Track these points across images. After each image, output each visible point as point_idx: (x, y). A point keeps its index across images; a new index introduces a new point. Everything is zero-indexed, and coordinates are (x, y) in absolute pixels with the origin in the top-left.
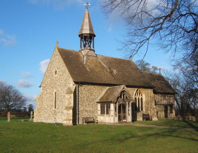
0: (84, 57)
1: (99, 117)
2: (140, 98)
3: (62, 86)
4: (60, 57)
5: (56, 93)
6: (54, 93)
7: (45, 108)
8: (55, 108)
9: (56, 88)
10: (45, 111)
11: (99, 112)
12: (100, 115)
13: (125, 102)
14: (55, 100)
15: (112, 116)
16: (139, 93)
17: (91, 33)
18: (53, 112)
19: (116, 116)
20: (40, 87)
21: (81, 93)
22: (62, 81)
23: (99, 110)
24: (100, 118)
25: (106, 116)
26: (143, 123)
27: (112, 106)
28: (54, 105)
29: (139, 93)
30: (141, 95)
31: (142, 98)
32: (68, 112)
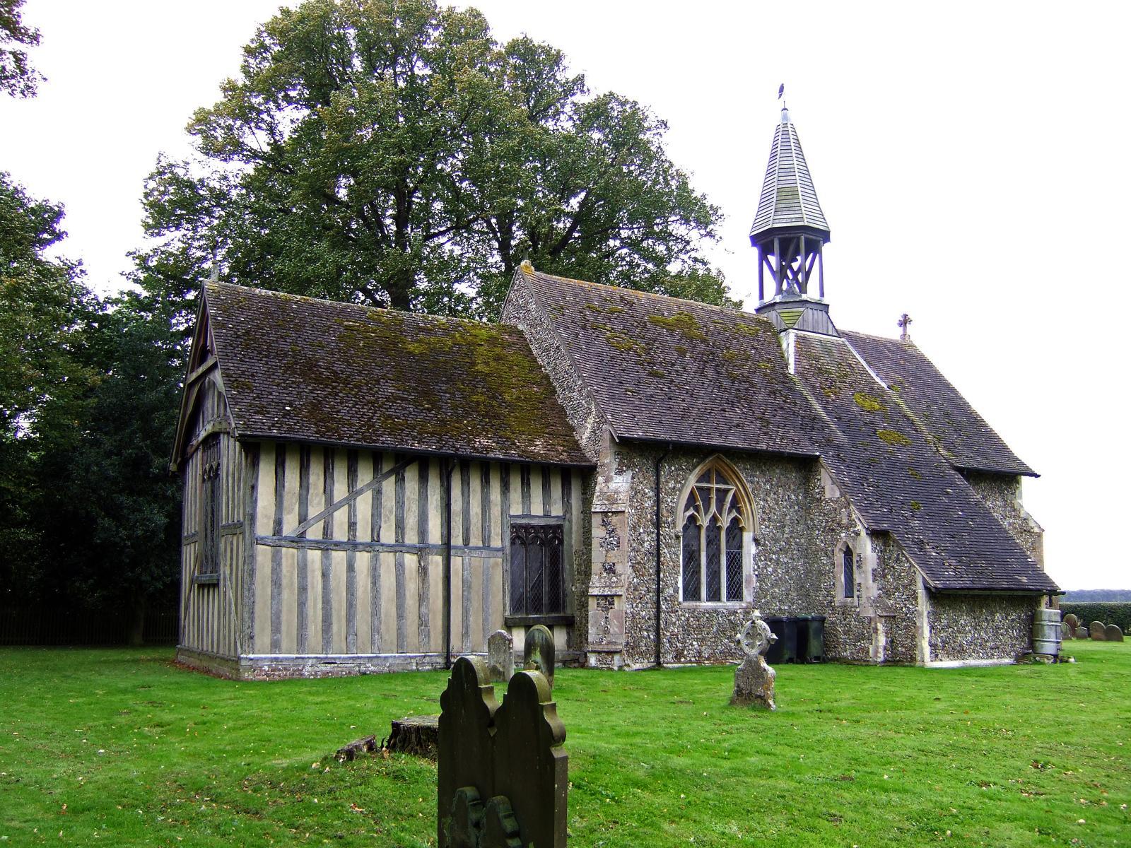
2: (725, 522)
16: (714, 496)
17: (184, 542)
29: (714, 496)
30: (735, 504)
31: (735, 521)
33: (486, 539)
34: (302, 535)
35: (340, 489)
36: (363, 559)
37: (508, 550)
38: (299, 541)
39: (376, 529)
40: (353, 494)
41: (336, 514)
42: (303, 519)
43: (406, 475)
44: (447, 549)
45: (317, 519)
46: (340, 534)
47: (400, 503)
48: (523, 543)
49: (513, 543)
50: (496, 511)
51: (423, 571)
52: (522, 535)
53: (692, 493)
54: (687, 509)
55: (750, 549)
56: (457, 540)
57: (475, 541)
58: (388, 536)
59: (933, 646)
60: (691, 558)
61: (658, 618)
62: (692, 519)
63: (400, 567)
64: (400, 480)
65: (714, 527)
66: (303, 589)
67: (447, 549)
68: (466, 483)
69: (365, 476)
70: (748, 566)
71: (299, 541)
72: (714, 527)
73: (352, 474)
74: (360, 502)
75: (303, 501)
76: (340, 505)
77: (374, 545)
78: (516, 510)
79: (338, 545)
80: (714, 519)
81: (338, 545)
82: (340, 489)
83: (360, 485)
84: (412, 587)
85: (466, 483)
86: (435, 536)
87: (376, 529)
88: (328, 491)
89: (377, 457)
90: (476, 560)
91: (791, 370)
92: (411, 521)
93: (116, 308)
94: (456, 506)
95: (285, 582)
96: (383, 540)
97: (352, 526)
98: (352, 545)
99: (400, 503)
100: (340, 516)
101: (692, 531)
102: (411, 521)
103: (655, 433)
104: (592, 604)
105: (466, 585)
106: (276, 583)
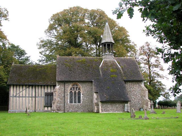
2: (77, 92)
31: (79, 91)
33: (41, 95)
34: (16, 96)
35: (21, 90)
36: (24, 98)
37: (44, 97)
38: (16, 96)
39: (26, 95)
40: (23, 90)
41: (19, 92)
42: (16, 94)
43: (49, 88)
44: (35, 97)
45: (18, 94)
46: (21, 95)
47: (29, 91)
48: (47, 96)
49: (45, 96)
50: (43, 92)
51: (32, 100)
52: (47, 94)
53: (71, 87)
54: (70, 90)
55: (82, 95)
56: (37, 96)
57: (40, 96)
58: (27, 95)
59: (102, 110)
60: (71, 97)
61: (64, 105)
62: (71, 91)
63: (29, 99)
64: (29, 88)
65: (75, 93)
66: (16, 102)
67: (35, 97)
68: (38, 88)
69: (24, 88)
70: (81, 98)
71: (16, 96)
72: (75, 93)
73: (23, 88)
74: (24, 92)
75: (16, 92)
76: (21, 92)
77: (26, 97)
78: (46, 91)
79: (21, 97)
80: (75, 91)
81: (21, 97)
82: (21, 90)
83: (24, 89)
84: (31, 102)
85: (38, 88)
86: (34, 95)
87: (26, 95)
88: (19, 90)
89: (26, 86)
90: (40, 98)
91: (100, 66)
92: (31, 93)
93: (168, 56)
94: (37, 91)
95: (14, 102)
96: (27, 96)
97: (22, 94)
98: (23, 97)
99: (29, 91)
100: (21, 93)
101: (71, 93)
102: (31, 93)
103: (63, 79)
104: (52, 104)
105: (38, 102)
106: (13, 102)
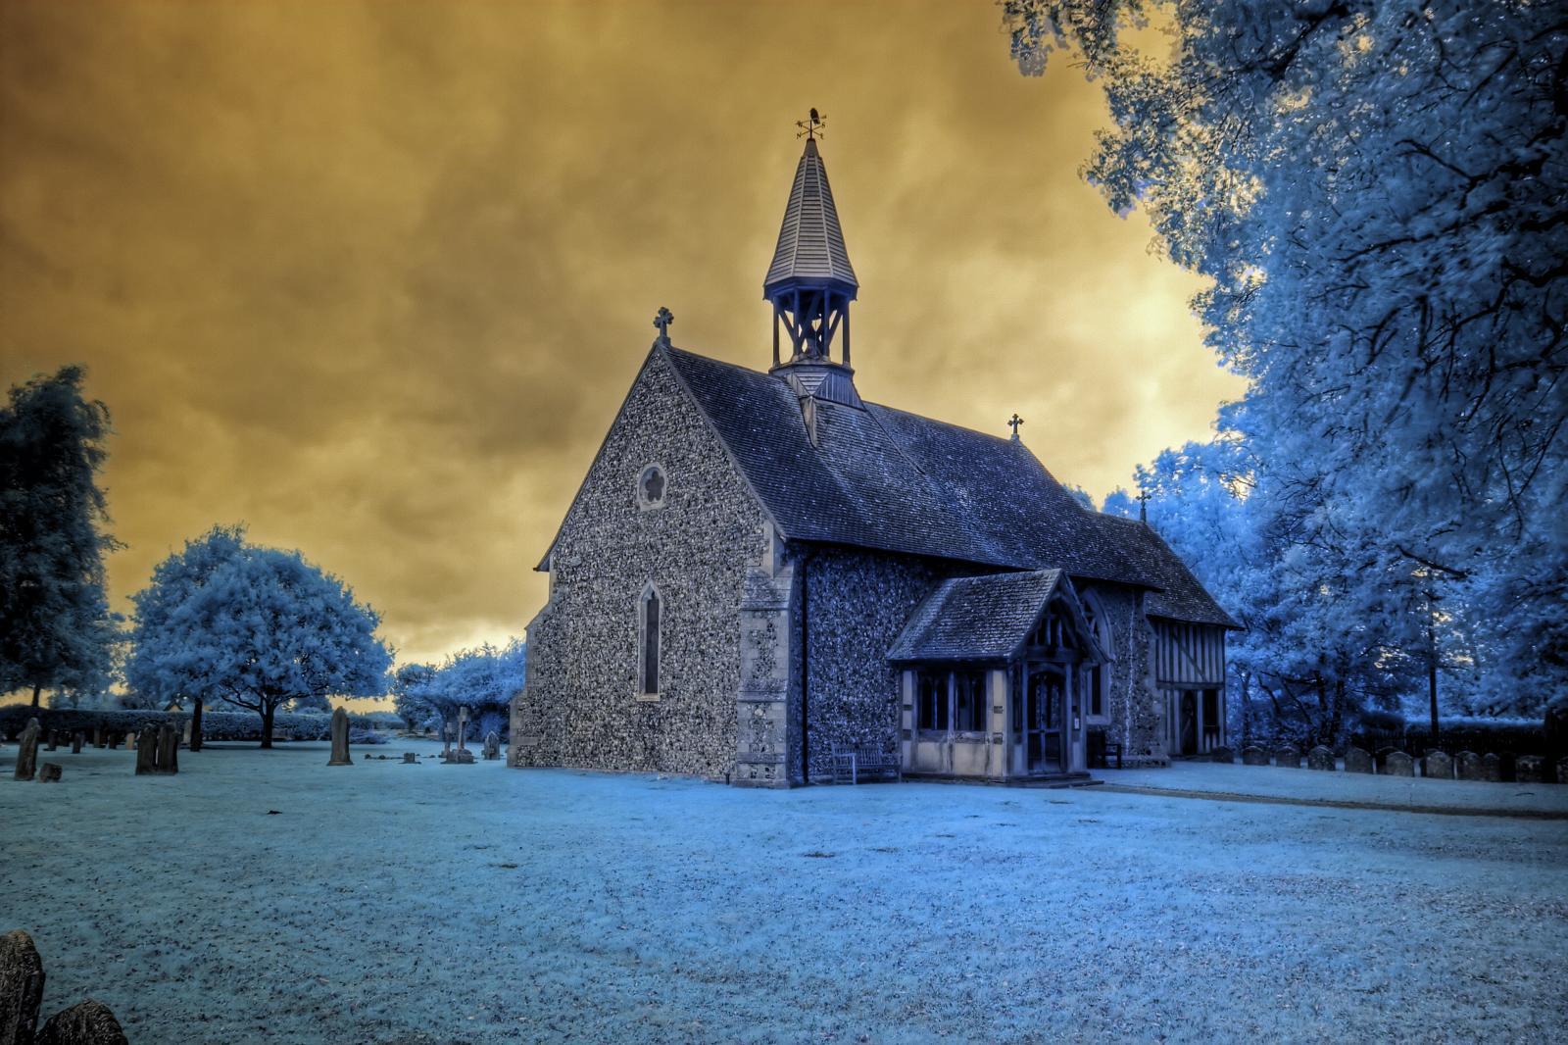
0: (802, 405)
1: (907, 746)
3: (703, 563)
4: (688, 396)
5: (652, 604)
6: (640, 606)
7: (580, 693)
8: (651, 688)
9: (655, 574)
10: (574, 709)
11: (909, 719)
12: (914, 735)
13: (1062, 665)
14: (651, 644)
15: (998, 741)
18: (634, 710)
19: (1019, 741)
20: (543, 567)
21: (818, 608)
22: (701, 535)
23: (908, 707)
24: (914, 750)
25: (960, 740)
26: (1055, 705)
27: (998, 689)
28: (640, 670)
32: (759, 712)
